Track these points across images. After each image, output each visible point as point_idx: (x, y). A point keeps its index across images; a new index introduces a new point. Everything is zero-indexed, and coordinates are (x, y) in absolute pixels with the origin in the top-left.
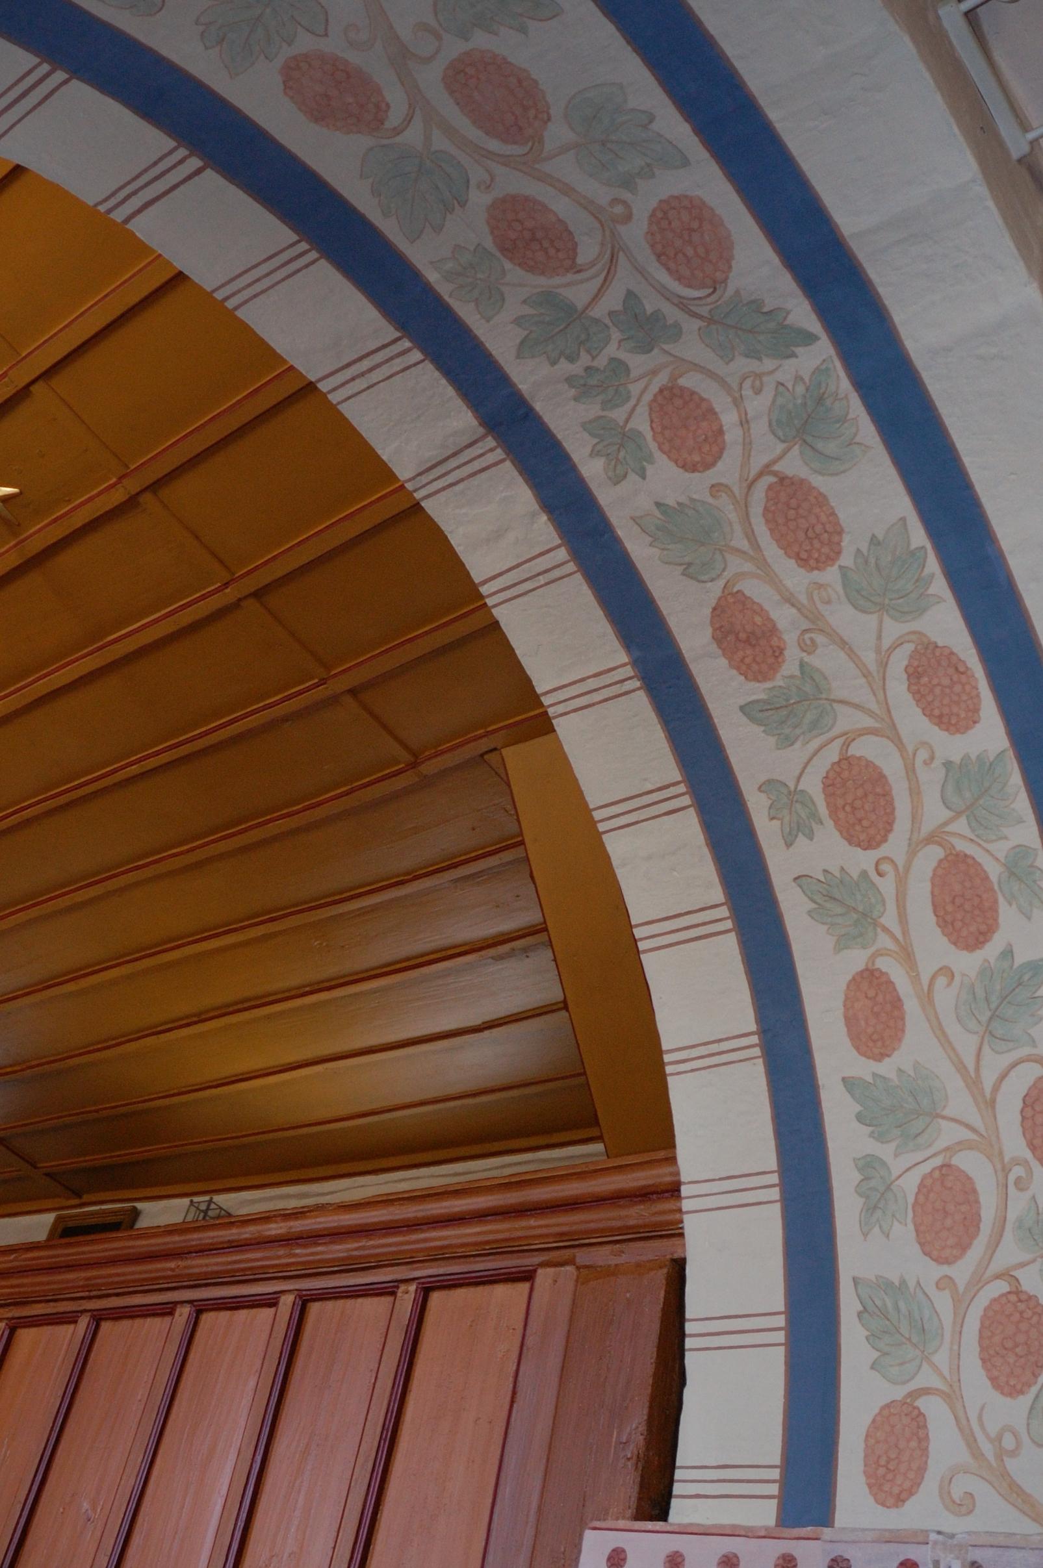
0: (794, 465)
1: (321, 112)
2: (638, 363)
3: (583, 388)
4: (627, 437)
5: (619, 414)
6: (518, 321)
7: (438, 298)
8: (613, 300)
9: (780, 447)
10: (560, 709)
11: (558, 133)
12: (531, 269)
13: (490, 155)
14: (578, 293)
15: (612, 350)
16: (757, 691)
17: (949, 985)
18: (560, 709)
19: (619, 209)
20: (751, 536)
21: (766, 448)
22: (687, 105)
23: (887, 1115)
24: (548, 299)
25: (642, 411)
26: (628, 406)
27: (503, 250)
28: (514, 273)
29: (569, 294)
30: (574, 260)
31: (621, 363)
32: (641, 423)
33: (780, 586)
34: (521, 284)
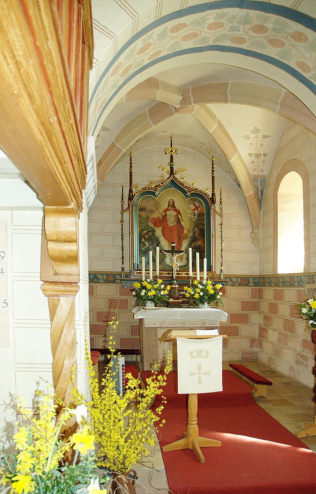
0: (199, 37)
1: (301, 34)
2: (230, 25)
3: (234, 17)
4: (222, 17)
5: (225, 18)
6: (252, 17)
7: (267, 12)
8: (241, 29)
9: (202, 36)
10: (45, 322)
11: (266, 42)
12: (256, 25)
13: (273, 36)
14: (247, 27)
15: (235, 23)
16: (168, 29)
17: (74, 444)
18: (45, 322)
19: (251, 39)
20: (193, 30)
21: (204, 35)
22: (252, 52)
23: (143, 462)
24: (250, 23)
25: (223, 22)
26: (225, 20)
27: (262, 25)
28: (258, 23)
29: (248, 26)
30: (251, 30)
31: (232, 23)
32: (222, 20)
33: (183, 33)
34: (256, 22)
